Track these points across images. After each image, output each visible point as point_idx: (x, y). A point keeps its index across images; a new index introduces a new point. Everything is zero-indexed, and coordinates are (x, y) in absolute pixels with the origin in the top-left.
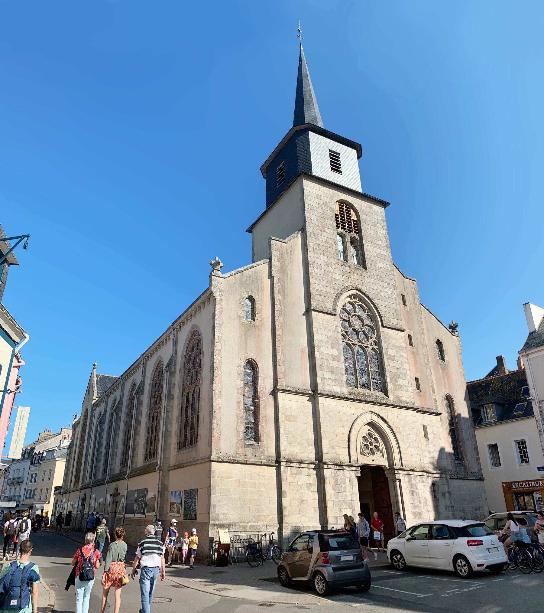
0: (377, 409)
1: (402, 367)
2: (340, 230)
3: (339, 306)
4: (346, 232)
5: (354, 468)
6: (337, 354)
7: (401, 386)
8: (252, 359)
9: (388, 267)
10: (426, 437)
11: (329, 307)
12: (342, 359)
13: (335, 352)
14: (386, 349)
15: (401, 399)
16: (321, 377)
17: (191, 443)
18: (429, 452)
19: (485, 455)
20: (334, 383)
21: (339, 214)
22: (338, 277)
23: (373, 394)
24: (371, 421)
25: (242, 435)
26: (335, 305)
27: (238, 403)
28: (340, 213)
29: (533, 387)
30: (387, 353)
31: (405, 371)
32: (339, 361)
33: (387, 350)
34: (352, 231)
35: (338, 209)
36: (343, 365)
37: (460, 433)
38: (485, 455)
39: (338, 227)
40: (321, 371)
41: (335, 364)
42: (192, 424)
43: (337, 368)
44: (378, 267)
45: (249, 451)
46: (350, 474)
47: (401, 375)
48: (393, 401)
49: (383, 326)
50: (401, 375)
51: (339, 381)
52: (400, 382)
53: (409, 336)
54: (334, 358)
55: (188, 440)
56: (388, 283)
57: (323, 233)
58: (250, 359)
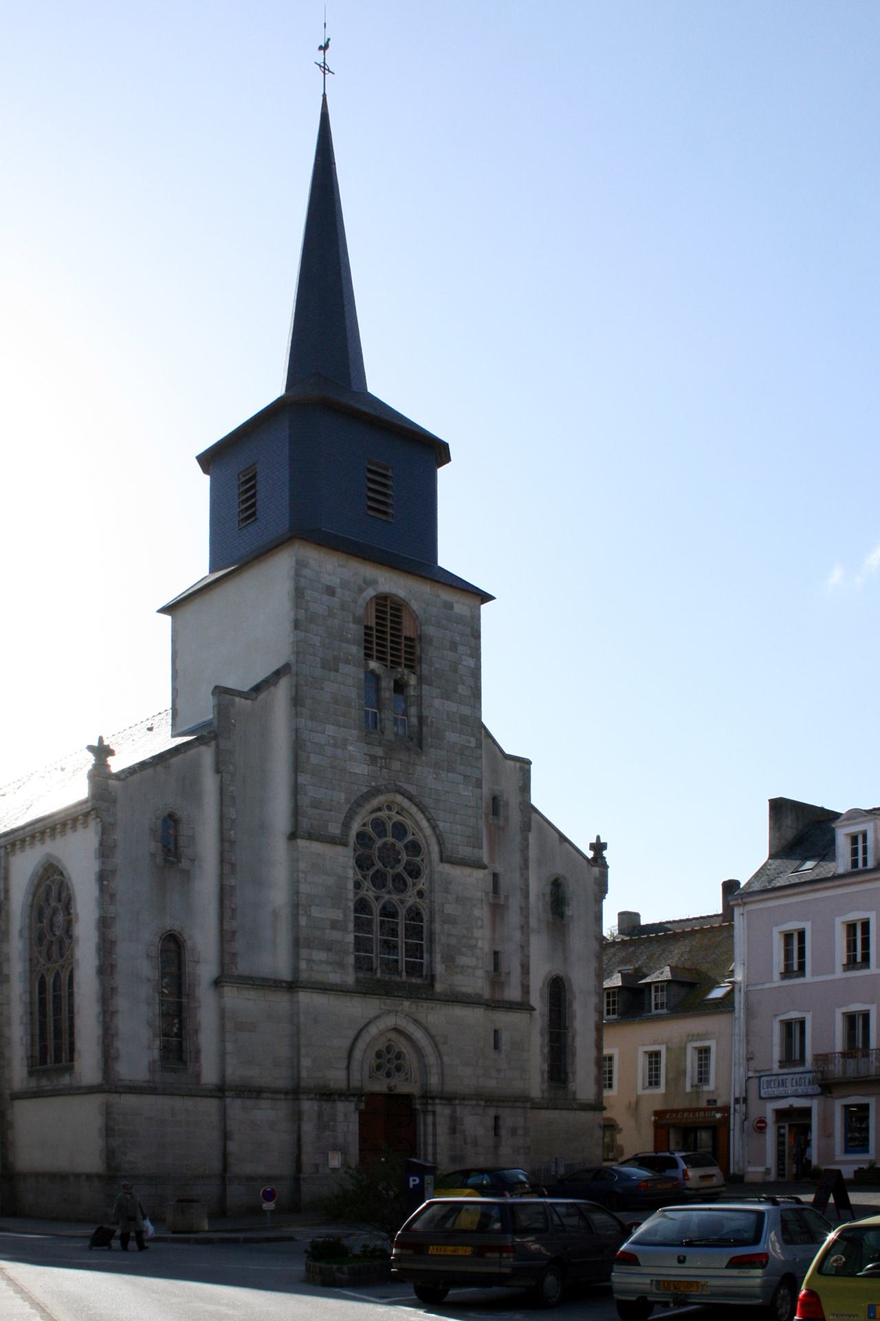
3: (356, 827)
4: (386, 666)
6: (341, 917)
7: (462, 967)
9: (469, 742)
11: (335, 829)
12: (351, 926)
13: (337, 915)
14: (443, 905)
15: (458, 989)
16: (307, 960)
17: (58, 1059)
18: (498, 1071)
19: (783, 1124)
20: (329, 968)
21: (374, 625)
23: (403, 982)
26: (346, 825)
28: (377, 624)
29: (742, 962)
30: (443, 911)
31: (473, 942)
33: (443, 906)
34: (399, 664)
35: (374, 614)
36: (350, 938)
37: (570, 1039)
38: (783, 1124)
39: (368, 656)
40: (309, 950)
41: (336, 935)
42: (57, 999)
44: (449, 742)
47: (464, 950)
49: (442, 861)
50: (464, 950)
51: (341, 965)
52: (463, 960)
53: (495, 876)
54: (335, 925)
55: (51, 1056)
56: (464, 776)
57: (333, 674)
58: (170, 931)
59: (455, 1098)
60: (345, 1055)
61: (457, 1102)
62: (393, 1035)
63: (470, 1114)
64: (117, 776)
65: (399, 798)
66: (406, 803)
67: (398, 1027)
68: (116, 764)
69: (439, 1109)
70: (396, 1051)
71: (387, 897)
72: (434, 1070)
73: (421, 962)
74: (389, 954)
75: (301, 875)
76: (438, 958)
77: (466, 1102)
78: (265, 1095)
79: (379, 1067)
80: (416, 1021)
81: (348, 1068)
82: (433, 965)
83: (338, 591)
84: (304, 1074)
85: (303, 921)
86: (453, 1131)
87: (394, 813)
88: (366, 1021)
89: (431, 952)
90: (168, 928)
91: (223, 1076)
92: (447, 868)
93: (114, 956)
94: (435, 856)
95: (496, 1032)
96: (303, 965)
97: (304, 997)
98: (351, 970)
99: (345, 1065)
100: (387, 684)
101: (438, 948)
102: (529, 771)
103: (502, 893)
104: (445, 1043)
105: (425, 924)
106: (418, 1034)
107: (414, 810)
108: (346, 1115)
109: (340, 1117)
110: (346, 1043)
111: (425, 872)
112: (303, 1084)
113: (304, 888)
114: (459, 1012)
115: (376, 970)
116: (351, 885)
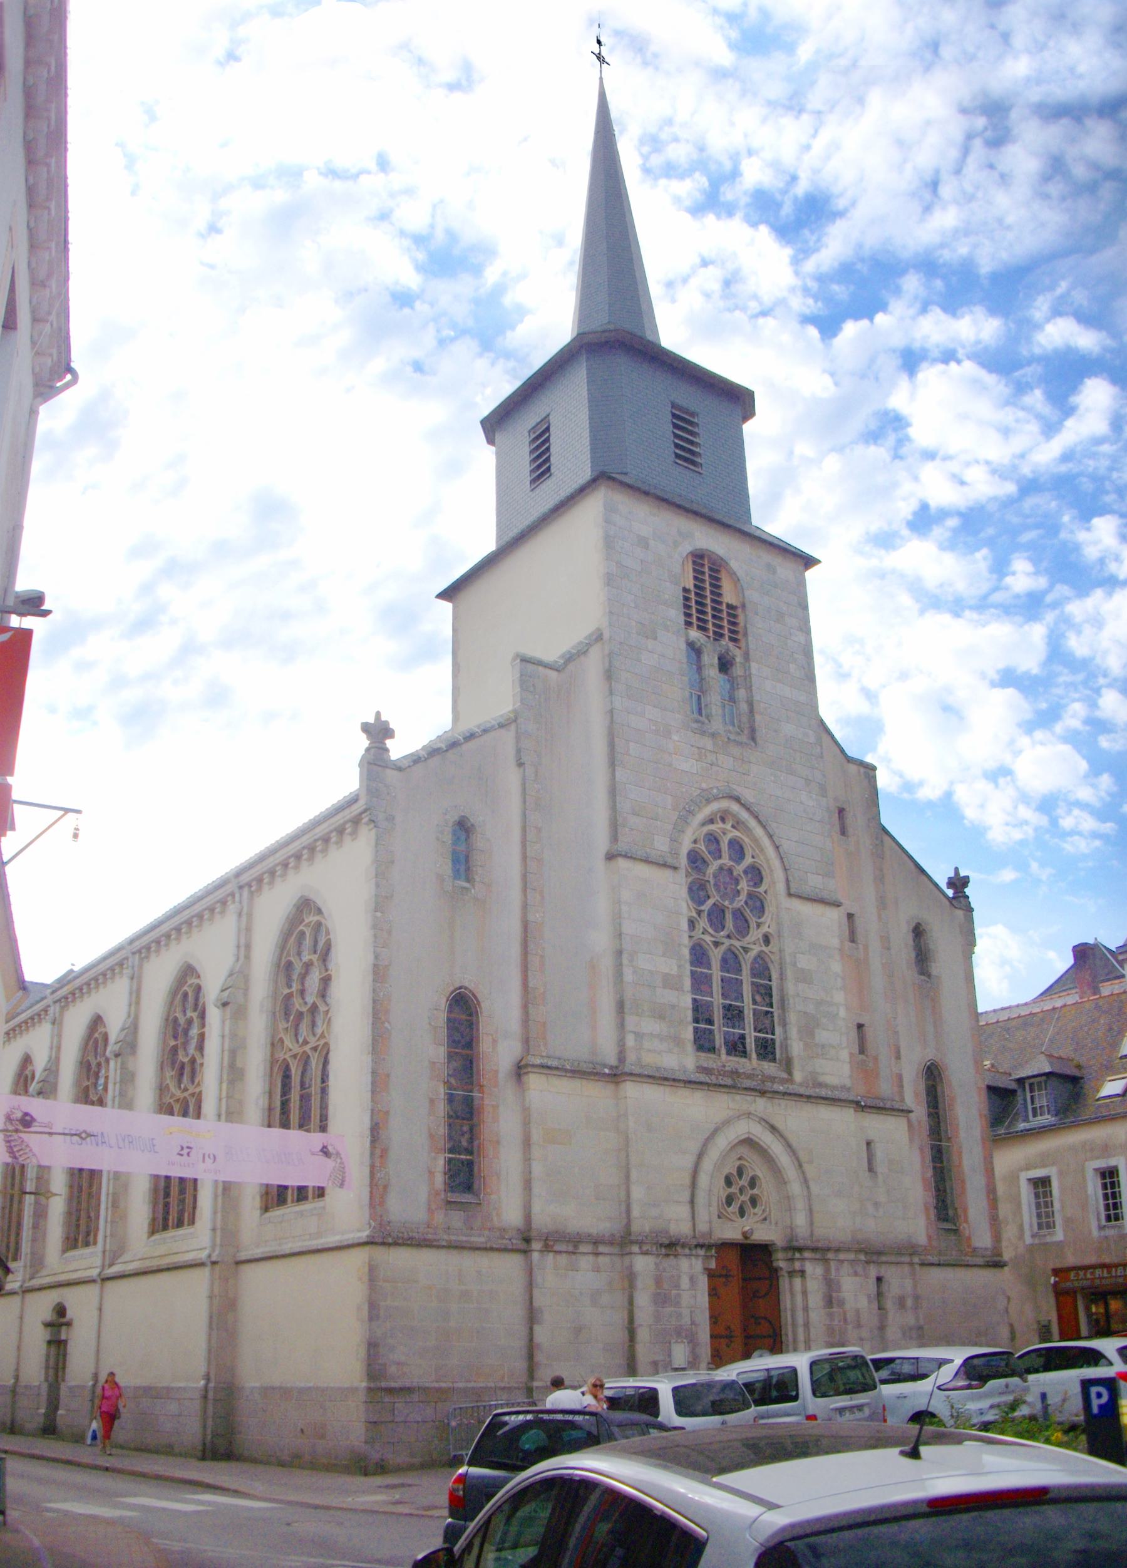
0: (761, 1105)
1: (828, 999)
2: (694, 634)
4: (708, 637)
5: (701, 1252)
7: (823, 1046)
8: (466, 988)
10: (871, 1169)
11: (661, 845)
12: (687, 983)
15: (821, 1079)
21: (692, 588)
22: (688, 765)
24: (747, 1136)
25: (439, 1180)
27: (432, 1101)
32: (679, 989)
33: (795, 957)
41: (668, 996)
43: (673, 1007)
45: (457, 1219)
46: (691, 1265)
47: (824, 1020)
48: (801, 1085)
49: (790, 895)
56: (806, 780)
57: (650, 644)
58: (460, 988)
59: (828, 1249)
60: (687, 1181)
61: (830, 1255)
62: (743, 1151)
63: (849, 1275)
64: (398, 767)
65: (735, 807)
66: (744, 815)
67: (751, 1136)
68: (398, 749)
69: (809, 1267)
70: (750, 1175)
71: (727, 942)
72: (800, 1205)
73: (772, 1039)
74: (733, 1027)
75: (624, 908)
76: (793, 1032)
77: (842, 1256)
78: (583, 1248)
79: (729, 1200)
80: (773, 1129)
81: (692, 1202)
82: (789, 1042)
83: (651, 542)
84: (636, 1212)
85: (628, 976)
86: (829, 1302)
87: (728, 826)
88: (712, 1127)
89: (784, 1024)
90: (457, 985)
91: (528, 1218)
92: (796, 904)
93: (386, 1025)
94: (781, 887)
95: (868, 1144)
96: (630, 1041)
97: (632, 1090)
98: (690, 1047)
99: (686, 1196)
100: (710, 659)
101: (792, 1017)
102: (875, 777)
103: (860, 937)
104: (810, 1162)
105: (774, 984)
106: (776, 1148)
107: (752, 823)
108: (692, 1279)
109: (685, 1283)
110: (689, 1161)
111: (770, 909)
112: (635, 1228)
113: (628, 928)
114: (825, 1113)
115: (719, 1050)
116: (685, 926)
